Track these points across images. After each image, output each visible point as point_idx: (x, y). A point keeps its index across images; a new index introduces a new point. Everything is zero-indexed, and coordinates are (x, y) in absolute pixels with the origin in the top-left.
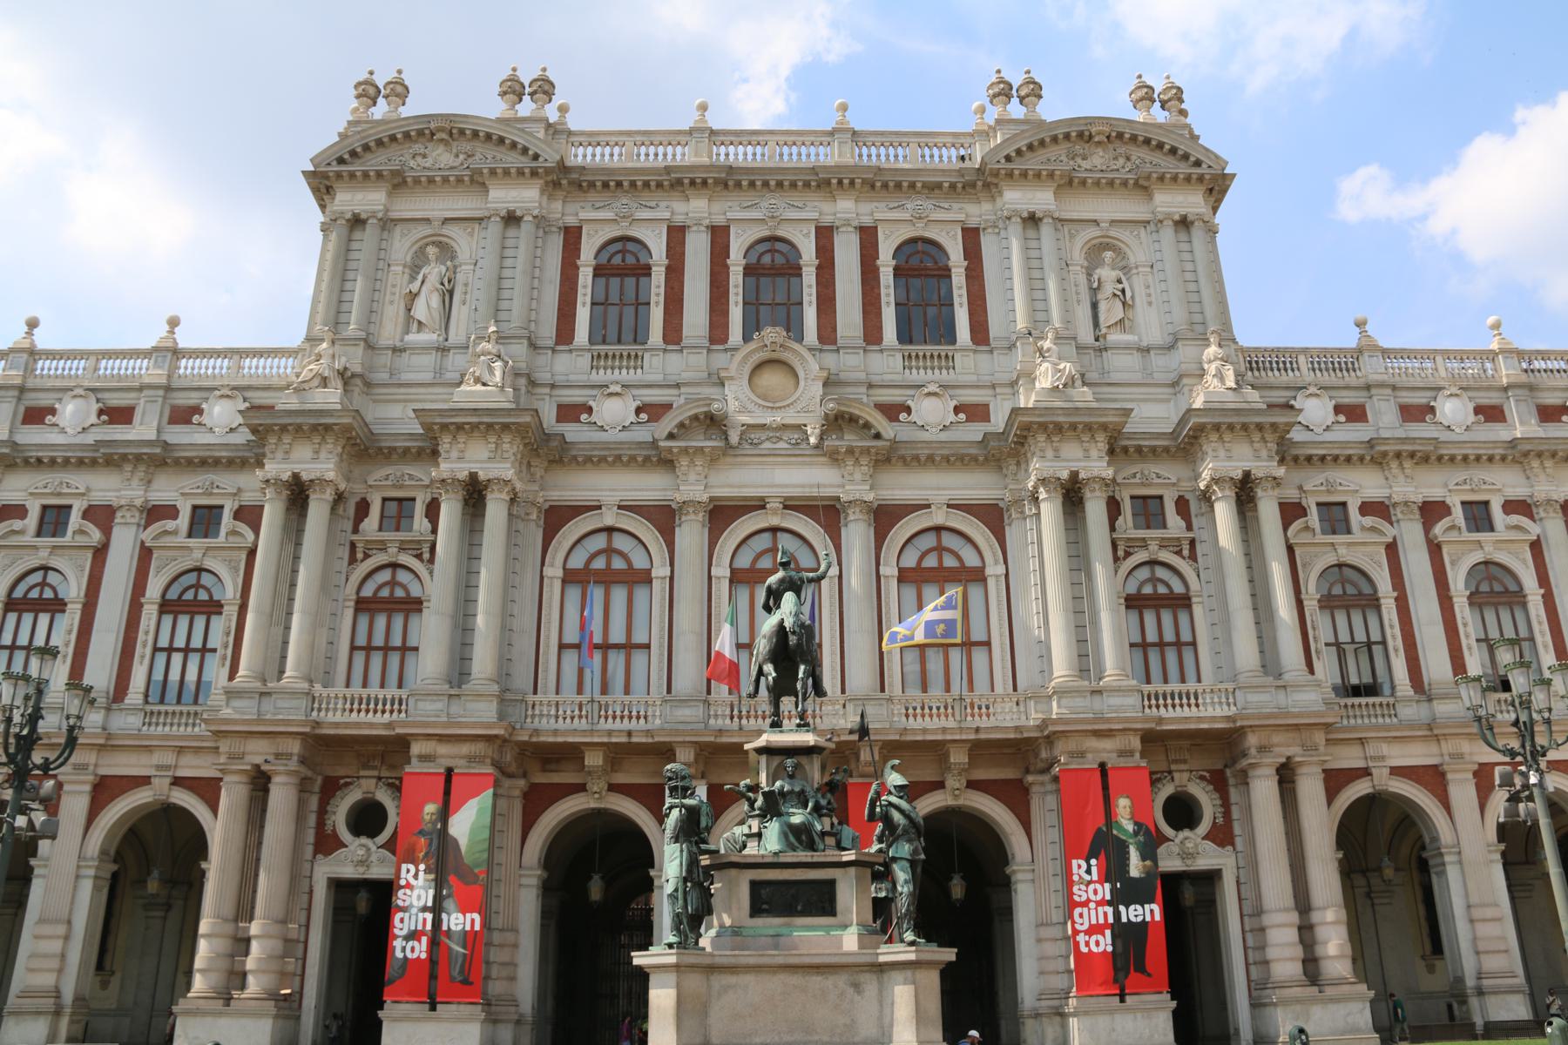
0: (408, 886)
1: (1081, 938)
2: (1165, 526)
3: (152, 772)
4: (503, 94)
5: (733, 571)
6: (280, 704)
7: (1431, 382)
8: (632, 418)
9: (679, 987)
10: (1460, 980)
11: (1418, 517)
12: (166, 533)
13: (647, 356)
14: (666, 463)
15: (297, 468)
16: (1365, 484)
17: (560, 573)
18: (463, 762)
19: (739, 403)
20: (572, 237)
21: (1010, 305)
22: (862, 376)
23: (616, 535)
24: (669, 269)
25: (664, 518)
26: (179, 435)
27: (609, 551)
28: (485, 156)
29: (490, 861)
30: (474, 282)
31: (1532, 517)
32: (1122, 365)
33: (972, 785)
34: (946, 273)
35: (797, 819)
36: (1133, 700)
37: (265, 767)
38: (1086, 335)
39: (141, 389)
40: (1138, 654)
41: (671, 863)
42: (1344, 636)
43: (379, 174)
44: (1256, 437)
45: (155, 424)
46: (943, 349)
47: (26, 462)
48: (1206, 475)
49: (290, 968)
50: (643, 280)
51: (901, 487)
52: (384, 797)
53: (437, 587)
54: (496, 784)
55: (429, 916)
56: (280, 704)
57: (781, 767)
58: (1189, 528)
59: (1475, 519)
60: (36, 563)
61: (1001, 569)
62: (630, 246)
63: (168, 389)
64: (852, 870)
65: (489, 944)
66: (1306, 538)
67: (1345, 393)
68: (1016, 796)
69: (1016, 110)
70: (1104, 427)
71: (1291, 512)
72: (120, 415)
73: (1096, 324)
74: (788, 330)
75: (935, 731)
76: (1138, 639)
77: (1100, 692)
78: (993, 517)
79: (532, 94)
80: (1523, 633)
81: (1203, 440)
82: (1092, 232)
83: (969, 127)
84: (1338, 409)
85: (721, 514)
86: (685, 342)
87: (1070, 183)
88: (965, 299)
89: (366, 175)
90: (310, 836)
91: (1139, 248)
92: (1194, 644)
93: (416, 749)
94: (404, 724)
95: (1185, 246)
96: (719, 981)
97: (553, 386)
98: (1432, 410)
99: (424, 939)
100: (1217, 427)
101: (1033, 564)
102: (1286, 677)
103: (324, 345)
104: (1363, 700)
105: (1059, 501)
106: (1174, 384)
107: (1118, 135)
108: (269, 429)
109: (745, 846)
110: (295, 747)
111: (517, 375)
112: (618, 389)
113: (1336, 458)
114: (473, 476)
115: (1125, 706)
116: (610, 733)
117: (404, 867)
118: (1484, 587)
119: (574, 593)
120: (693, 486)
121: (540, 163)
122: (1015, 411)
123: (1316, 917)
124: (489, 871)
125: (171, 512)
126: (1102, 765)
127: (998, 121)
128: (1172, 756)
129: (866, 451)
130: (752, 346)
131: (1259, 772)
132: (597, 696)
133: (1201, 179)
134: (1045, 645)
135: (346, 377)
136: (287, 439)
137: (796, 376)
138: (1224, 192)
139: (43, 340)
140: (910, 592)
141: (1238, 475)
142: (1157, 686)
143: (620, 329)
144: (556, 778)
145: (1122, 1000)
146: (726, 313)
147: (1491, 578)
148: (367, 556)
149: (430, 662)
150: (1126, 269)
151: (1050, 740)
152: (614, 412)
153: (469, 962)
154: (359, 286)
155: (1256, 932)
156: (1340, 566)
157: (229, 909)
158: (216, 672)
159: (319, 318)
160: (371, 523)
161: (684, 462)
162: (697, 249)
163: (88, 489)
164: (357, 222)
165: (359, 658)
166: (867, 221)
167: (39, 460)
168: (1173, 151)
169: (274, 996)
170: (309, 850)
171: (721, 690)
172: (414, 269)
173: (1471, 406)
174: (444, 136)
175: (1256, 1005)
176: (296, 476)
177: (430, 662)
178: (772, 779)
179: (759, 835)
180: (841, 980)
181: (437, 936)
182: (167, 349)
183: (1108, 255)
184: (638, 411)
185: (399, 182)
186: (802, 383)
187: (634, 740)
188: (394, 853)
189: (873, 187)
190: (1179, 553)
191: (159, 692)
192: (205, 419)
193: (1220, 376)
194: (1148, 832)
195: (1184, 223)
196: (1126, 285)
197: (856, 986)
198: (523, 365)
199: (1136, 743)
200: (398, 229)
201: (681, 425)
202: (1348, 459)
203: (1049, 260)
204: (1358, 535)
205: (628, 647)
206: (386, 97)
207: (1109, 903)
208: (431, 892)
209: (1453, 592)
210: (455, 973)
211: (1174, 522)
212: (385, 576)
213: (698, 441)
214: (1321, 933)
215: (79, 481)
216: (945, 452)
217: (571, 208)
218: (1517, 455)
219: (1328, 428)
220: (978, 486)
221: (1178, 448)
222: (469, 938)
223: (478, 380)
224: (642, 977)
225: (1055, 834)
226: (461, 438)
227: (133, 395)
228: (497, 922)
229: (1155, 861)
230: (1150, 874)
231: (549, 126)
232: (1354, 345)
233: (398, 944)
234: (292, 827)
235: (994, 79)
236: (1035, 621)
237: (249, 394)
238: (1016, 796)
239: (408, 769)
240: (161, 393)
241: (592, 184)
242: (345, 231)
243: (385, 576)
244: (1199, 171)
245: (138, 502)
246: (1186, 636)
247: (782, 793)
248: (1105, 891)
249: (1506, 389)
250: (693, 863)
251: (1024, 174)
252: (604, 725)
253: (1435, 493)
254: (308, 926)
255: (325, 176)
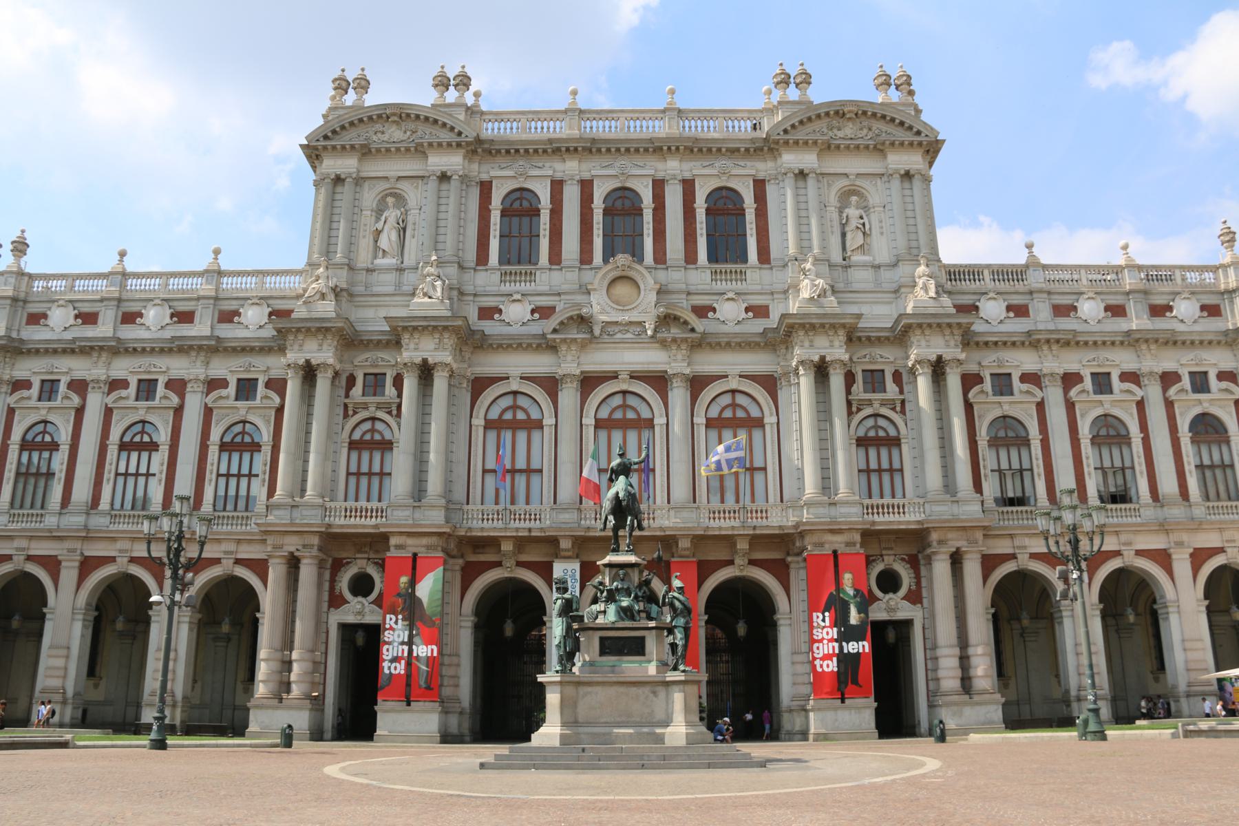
0: (391, 628)
1: (817, 663)
2: (885, 391)
3: (222, 556)
4: (436, 86)
5: (597, 420)
6: (305, 513)
7: (1075, 287)
8: (529, 316)
9: (561, 693)
10: (1067, 692)
11: (1060, 383)
12: (221, 397)
13: (538, 273)
14: (552, 348)
15: (308, 356)
16: (1026, 361)
17: (482, 422)
18: (423, 549)
19: (600, 307)
20: (486, 188)
21: (784, 239)
22: (684, 286)
23: (520, 397)
24: (552, 211)
25: (551, 385)
26: (226, 331)
27: (515, 407)
28: (426, 133)
29: (442, 613)
30: (420, 221)
31: (1139, 384)
32: (860, 278)
33: (752, 562)
34: (741, 213)
35: (624, 604)
36: (856, 510)
37: (296, 554)
38: (836, 257)
39: (198, 299)
40: (864, 477)
41: (556, 628)
42: (1004, 465)
43: (353, 147)
44: (947, 331)
45: (209, 323)
46: (738, 267)
47: (126, 350)
48: (912, 357)
49: (317, 680)
50: (534, 219)
51: (709, 363)
52: (372, 571)
53: (404, 436)
54: (445, 563)
55: (406, 648)
56: (305, 513)
57: (617, 575)
58: (901, 392)
59: (1100, 384)
60: (137, 418)
61: (774, 419)
62: (525, 194)
63: (216, 299)
64: (654, 632)
65: (442, 664)
66: (982, 398)
67: (1014, 297)
68: (781, 570)
69: (793, 94)
70: (843, 326)
71: (970, 381)
72: (185, 317)
73: (844, 249)
74: (633, 256)
75: (726, 529)
76: (863, 466)
77: (835, 504)
78: (770, 383)
79: (456, 86)
80: (1128, 464)
81: (911, 334)
82: (843, 182)
83: (760, 106)
84: (1009, 308)
85: (589, 383)
86: (564, 263)
87: (829, 147)
88: (754, 231)
89: (343, 147)
90: (326, 597)
91: (876, 194)
92: (901, 470)
93: (393, 541)
94: (384, 525)
95: (907, 192)
96: (583, 690)
97: (475, 295)
98: (1075, 308)
99: (403, 662)
100: (920, 326)
101: (795, 417)
102: (959, 495)
103: (321, 270)
104: (1014, 509)
105: (812, 376)
106: (896, 291)
107: (864, 113)
108: (289, 330)
109: (597, 618)
110: (315, 540)
111: (451, 289)
112: (519, 297)
113: (1005, 343)
114: (425, 361)
115: (851, 514)
116: (517, 530)
117: (388, 616)
118: (1103, 432)
119: (492, 435)
120: (570, 364)
121: (462, 138)
122: (783, 316)
123: (971, 651)
124: (441, 619)
125: (223, 383)
126: (835, 552)
127: (780, 103)
128: (883, 545)
129: (685, 340)
130: (609, 267)
131: (938, 557)
132: (509, 506)
133: (920, 144)
134: (801, 470)
135: (337, 292)
136: (300, 337)
137: (638, 287)
138: (937, 152)
139: (131, 266)
140: (713, 434)
141: (933, 358)
142: (876, 500)
143: (519, 254)
144: (482, 558)
145: (843, 702)
146: (591, 242)
147: (1108, 426)
148: (355, 413)
149: (400, 484)
150: (866, 208)
151: (802, 535)
152: (517, 312)
153: (430, 676)
154: (342, 227)
155: (933, 660)
156: (1004, 417)
157: (278, 643)
158: (259, 490)
159: (316, 249)
160: (357, 390)
161: (564, 347)
162: (572, 196)
163: (168, 369)
164: (339, 180)
165: (353, 480)
166: (688, 175)
167: (135, 349)
168: (902, 124)
169: (308, 697)
170: (326, 605)
171: (588, 503)
172: (379, 212)
173: (1102, 306)
174: (396, 118)
175: (931, 706)
176: (308, 361)
177: (400, 484)
178: (612, 580)
179: (605, 612)
180: (647, 690)
181: (410, 660)
182: (214, 271)
183: (854, 199)
184: (533, 312)
185: (366, 152)
186: (642, 292)
187: (533, 534)
188: (380, 607)
189: (692, 151)
190: (894, 409)
191: (222, 502)
192: (242, 319)
193: (925, 288)
194: (863, 596)
195: (907, 176)
196: (866, 220)
197: (654, 693)
198: (455, 282)
199: (858, 538)
200: (366, 184)
201: (562, 323)
202: (1014, 344)
203: (813, 204)
204: (1017, 397)
205: (529, 471)
206: (355, 89)
207: (836, 641)
208: (407, 633)
209: (1080, 436)
210: (422, 683)
211: (891, 387)
212: (367, 426)
213: (574, 334)
214: (974, 661)
215: (162, 362)
216: (739, 340)
217: (485, 168)
218: (1132, 340)
219: (1001, 322)
220: (760, 363)
221: (895, 337)
222: (430, 661)
223: (425, 295)
224: (542, 687)
225: (804, 596)
226: (416, 335)
227: (193, 303)
228: (446, 651)
229: (867, 614)
230: (863, 623)
231: (468, 108)
232: (1023, 262)
233: (386, 665)
234: (315, 592)
235: (778, 72)
236: (796, 455)
237: (270, 302)
238: (781, 570)
239: (388, 554)
240: (212, 301)
241: (499, 151)
242: (330, 187)
243: (367, 426)
244: (919, 139)
245: (202, 377)
246: (896, 465)
247: (617, 589)
248: (834, 633)
249: (1128, 294)
250: (569, 628)
251: (796, 143)
252: (513, 525)
253: (1073, 367)
254: (326, 653)
255: (315, 148)
